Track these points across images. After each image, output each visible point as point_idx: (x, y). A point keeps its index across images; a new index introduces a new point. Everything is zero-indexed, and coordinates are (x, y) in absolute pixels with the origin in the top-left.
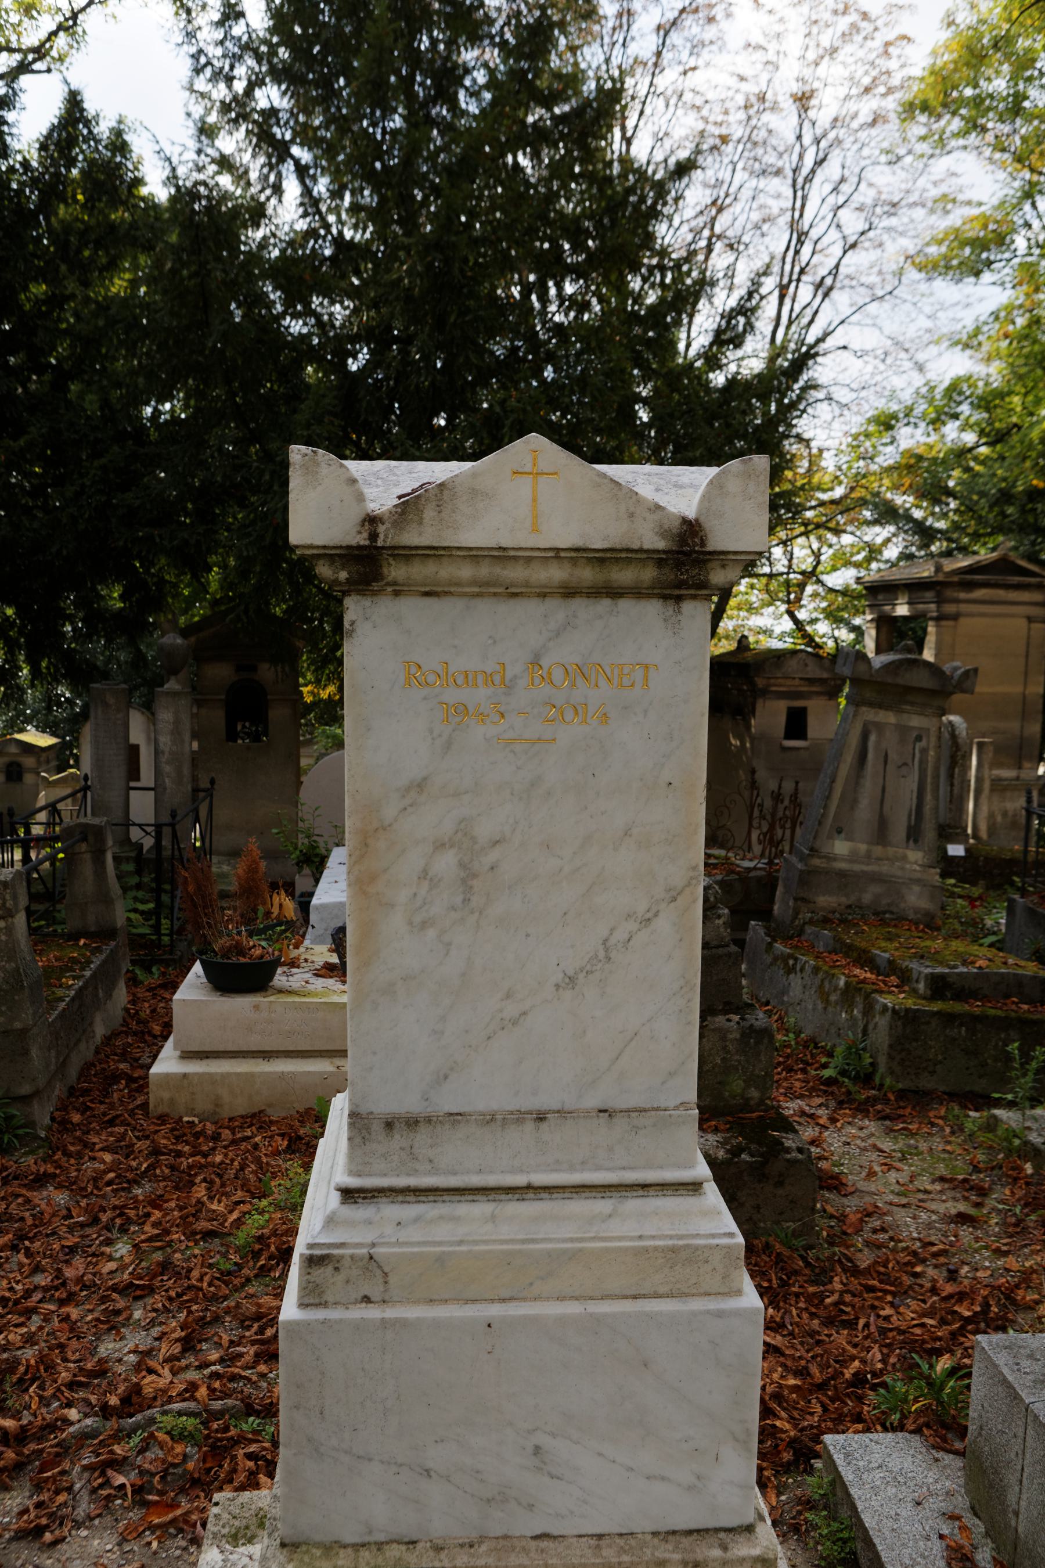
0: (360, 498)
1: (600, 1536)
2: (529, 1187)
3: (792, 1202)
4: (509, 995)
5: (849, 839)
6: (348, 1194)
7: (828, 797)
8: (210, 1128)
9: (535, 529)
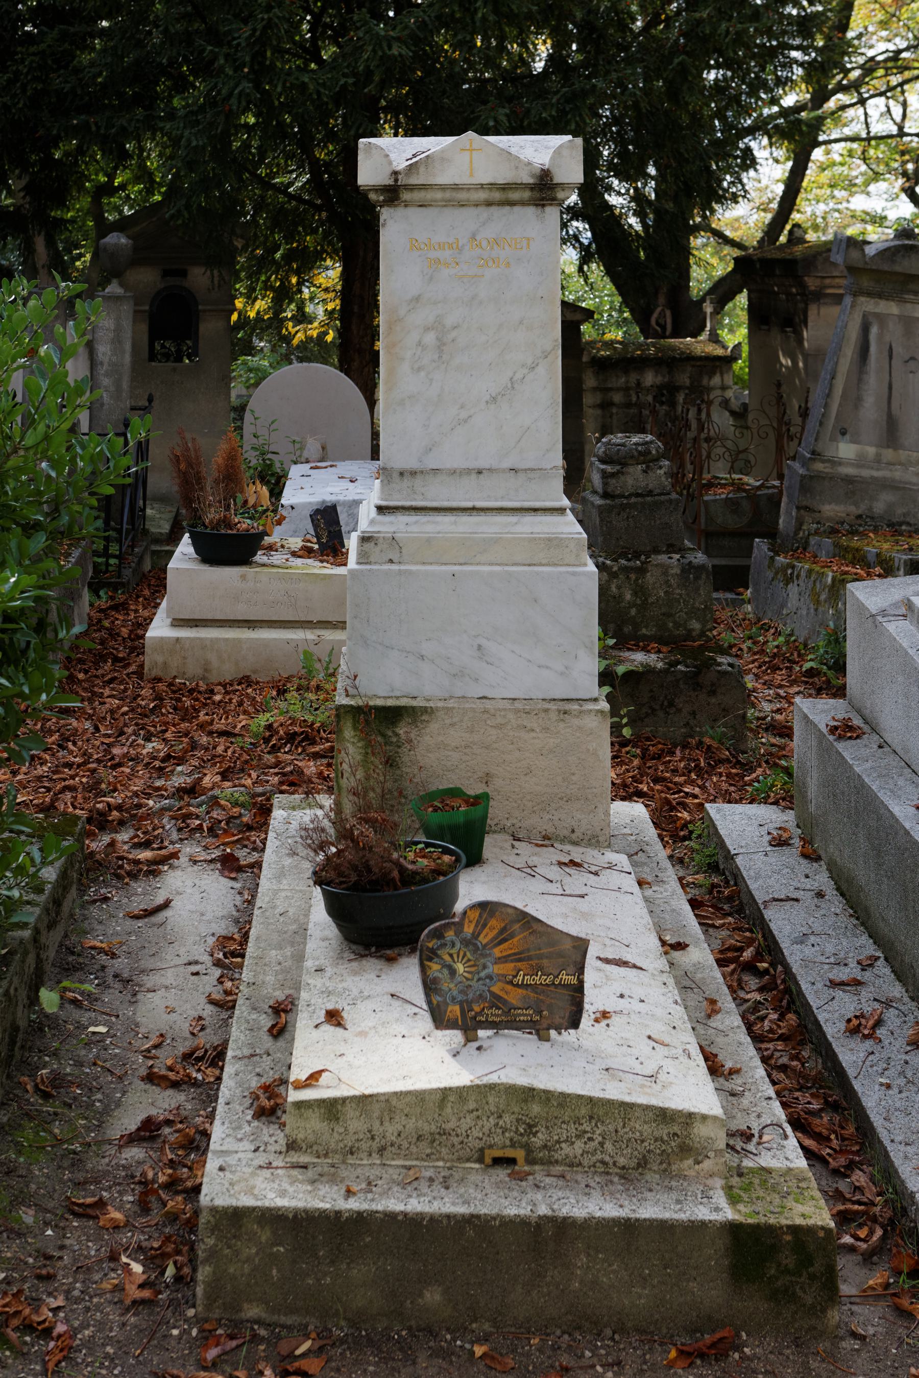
0: (390, 163)
1: (514, 699)
2: (474, 509)
3: (724, 710)
4: (462, 407)
5: (854, 441)
6: (381, 509)
7: (828, 395)
8: (203, 687)
9: (471, 175)
